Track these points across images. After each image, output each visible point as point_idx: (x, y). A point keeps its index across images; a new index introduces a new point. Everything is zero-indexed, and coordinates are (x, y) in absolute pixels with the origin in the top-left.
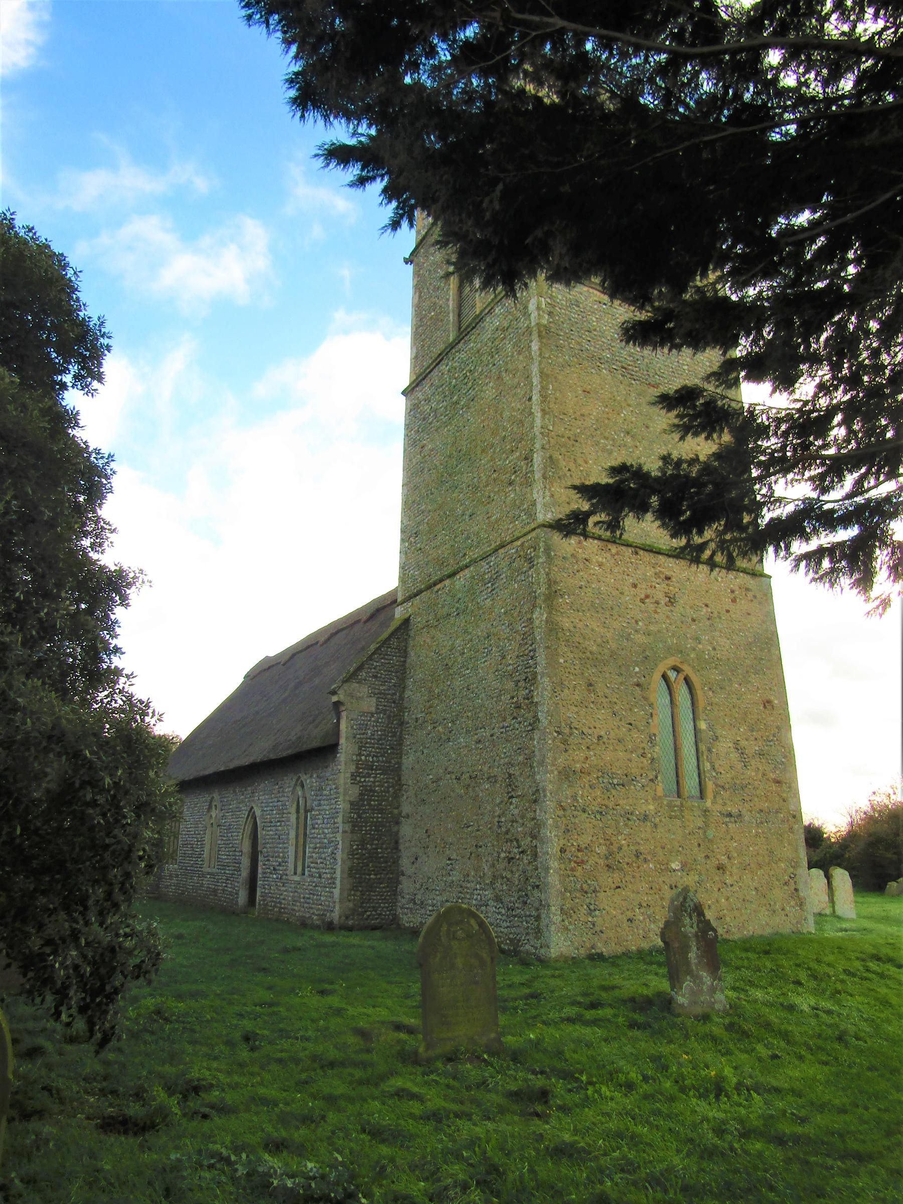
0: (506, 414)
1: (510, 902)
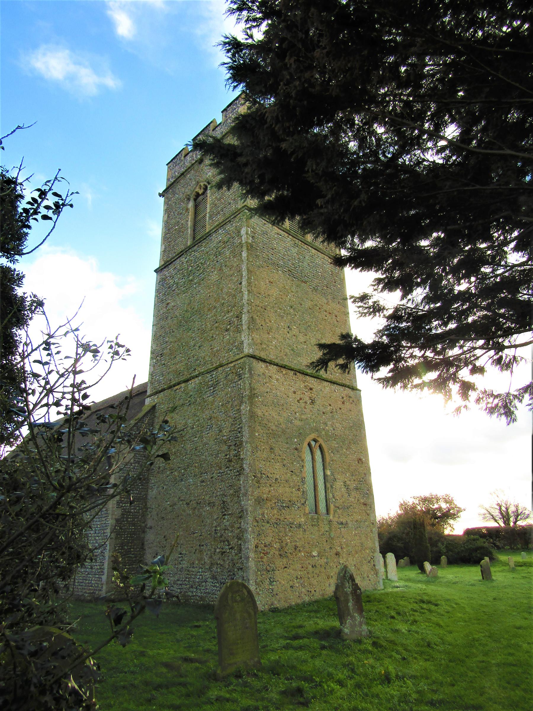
0: (225, 290)
1: (223, 579)
